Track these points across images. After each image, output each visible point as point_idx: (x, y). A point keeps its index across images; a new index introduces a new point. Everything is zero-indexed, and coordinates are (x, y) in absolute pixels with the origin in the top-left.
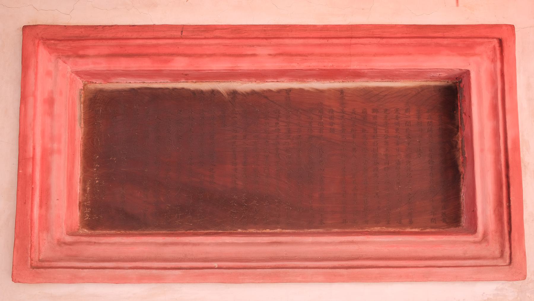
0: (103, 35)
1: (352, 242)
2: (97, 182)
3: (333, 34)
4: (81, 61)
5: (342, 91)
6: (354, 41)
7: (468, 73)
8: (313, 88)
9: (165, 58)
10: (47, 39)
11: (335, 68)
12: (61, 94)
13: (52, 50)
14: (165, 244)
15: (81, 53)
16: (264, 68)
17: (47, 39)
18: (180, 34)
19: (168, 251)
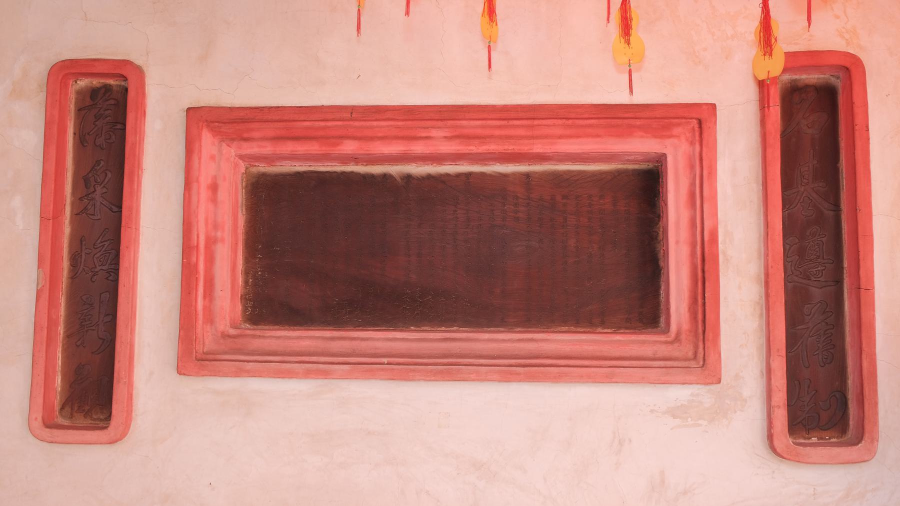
4: (245, 145)
6: (536, 122)
13: (215, 132)
14: (332, 339)
19: (336, 346)
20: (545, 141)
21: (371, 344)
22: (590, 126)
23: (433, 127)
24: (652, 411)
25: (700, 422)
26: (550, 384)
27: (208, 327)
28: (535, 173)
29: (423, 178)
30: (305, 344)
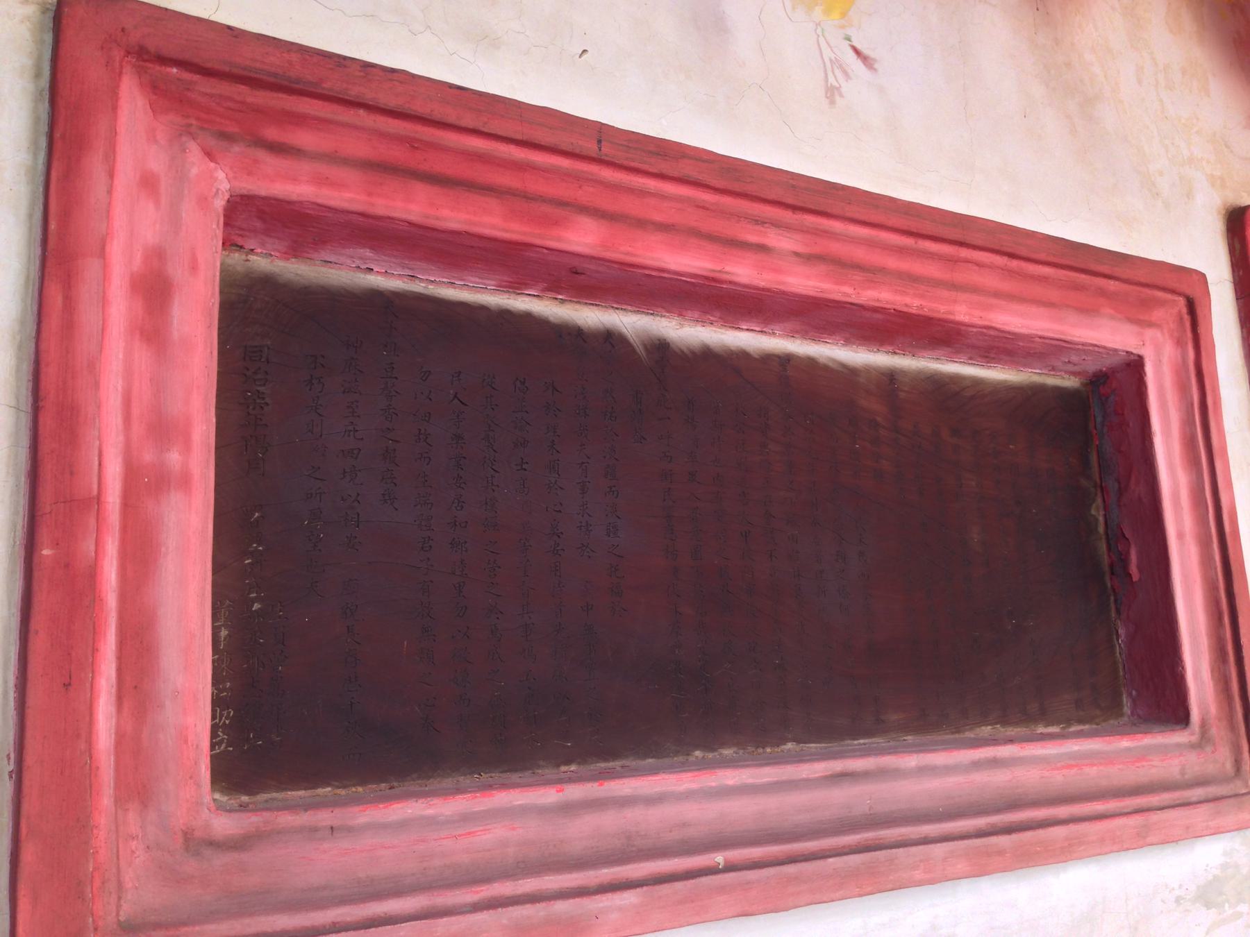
0: (368, 95)
1: (995, 763)
2: (256, 606)
3: (929, 228)
4: (271, 162)
5: (891, 377)
6: (964, 253)
7: (1135, 366)
8: (834, 361)
9: (547, 209)
10: (163, 60)
11: (926, 312)
12: (194, 268)
13: (164, 97)
14: (568, 809)
15: (272, 133)
16: (782, 288)
17: (163, 60)
18: (595, 147)
19: (580, 832)
20: (975, 298)
21: (669, 812)
22: (1043, 279)
23: (776, 224)
24: (1178, 900)
25: (1239, 909)
26: (1031, 870)
27: (132, 818)
28: (903, 372)
29: (693, 353)
30: (492, 838)
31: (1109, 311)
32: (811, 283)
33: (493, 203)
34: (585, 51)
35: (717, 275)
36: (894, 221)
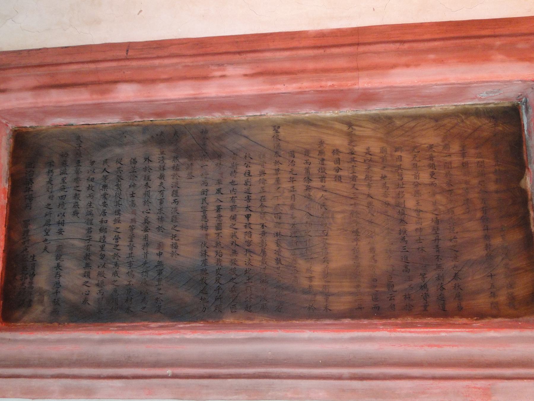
6: (362, 49)
14: (102, 342)
19: (106, 351)
31: (500, 57)
32: (256, 88)
33: (83, 89)
34: (141, 11)
35: (196, 96)
36: (304, 43)
